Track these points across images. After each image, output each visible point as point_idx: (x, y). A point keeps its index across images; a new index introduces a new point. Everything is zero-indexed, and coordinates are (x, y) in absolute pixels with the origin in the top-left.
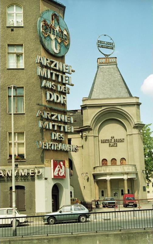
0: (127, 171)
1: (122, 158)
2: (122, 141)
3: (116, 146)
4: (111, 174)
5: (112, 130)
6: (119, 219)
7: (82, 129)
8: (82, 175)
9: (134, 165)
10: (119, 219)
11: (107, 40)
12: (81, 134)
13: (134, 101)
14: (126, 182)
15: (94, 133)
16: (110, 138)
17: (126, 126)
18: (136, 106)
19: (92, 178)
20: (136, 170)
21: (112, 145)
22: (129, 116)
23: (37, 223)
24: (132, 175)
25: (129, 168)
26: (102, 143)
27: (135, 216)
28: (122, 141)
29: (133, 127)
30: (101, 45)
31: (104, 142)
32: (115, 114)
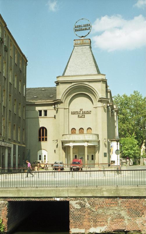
0: (87, 139)
1: (72, 128)
2: (89, 113)
3: (84, 117)
4: (74, 142)
5: (81, 103)
6: (18, 180)
7: (56, 101)
8: (53, 141)
9: (97, 134)
10: (46, 179)
11: (82, 23)
12: (53, 107)
13: (100, 77)
14: (86, 149)
15: (65, 105)
16: (79, 110)
17: (92, 98)
18: (101, 82)
19: (60, 145)
20: (98, 138)
21: (80, 116)
22: (93, 90)
23: (118, 177)
24: (92, 143)
25: (89, 137)
26: (72, 114)
27: (23, 178)
28: (89, 113)
29: (98, 101)
30: (78, 28)
31: (73, 113)
32: (83, 89)
